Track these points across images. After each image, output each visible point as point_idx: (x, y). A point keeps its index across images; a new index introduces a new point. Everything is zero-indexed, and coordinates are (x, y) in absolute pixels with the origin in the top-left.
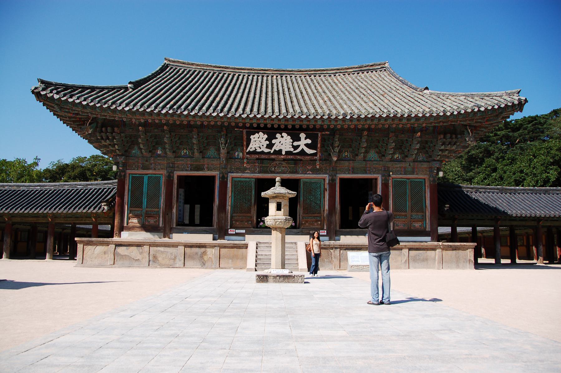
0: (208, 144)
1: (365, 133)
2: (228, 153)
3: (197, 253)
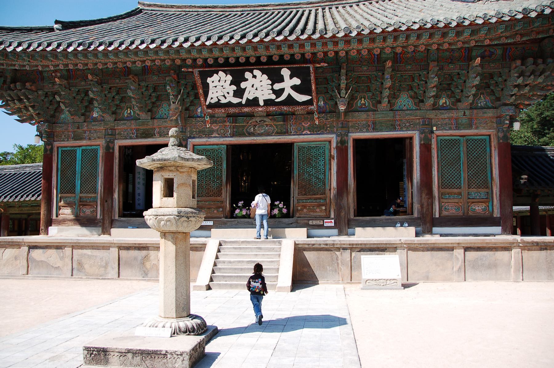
1: (389, 64)
3: (135, 259)
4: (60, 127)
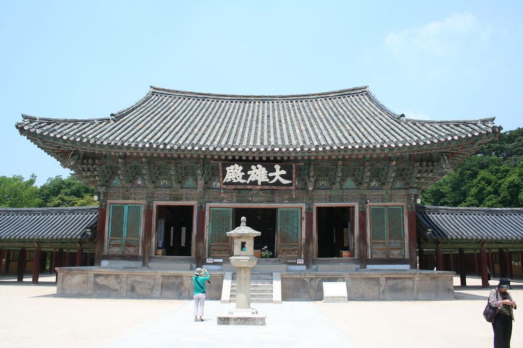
0: (186, 174)
1: (340, 163)
2: (206, 183)
3: (174, 284)
4: (113, 190)
